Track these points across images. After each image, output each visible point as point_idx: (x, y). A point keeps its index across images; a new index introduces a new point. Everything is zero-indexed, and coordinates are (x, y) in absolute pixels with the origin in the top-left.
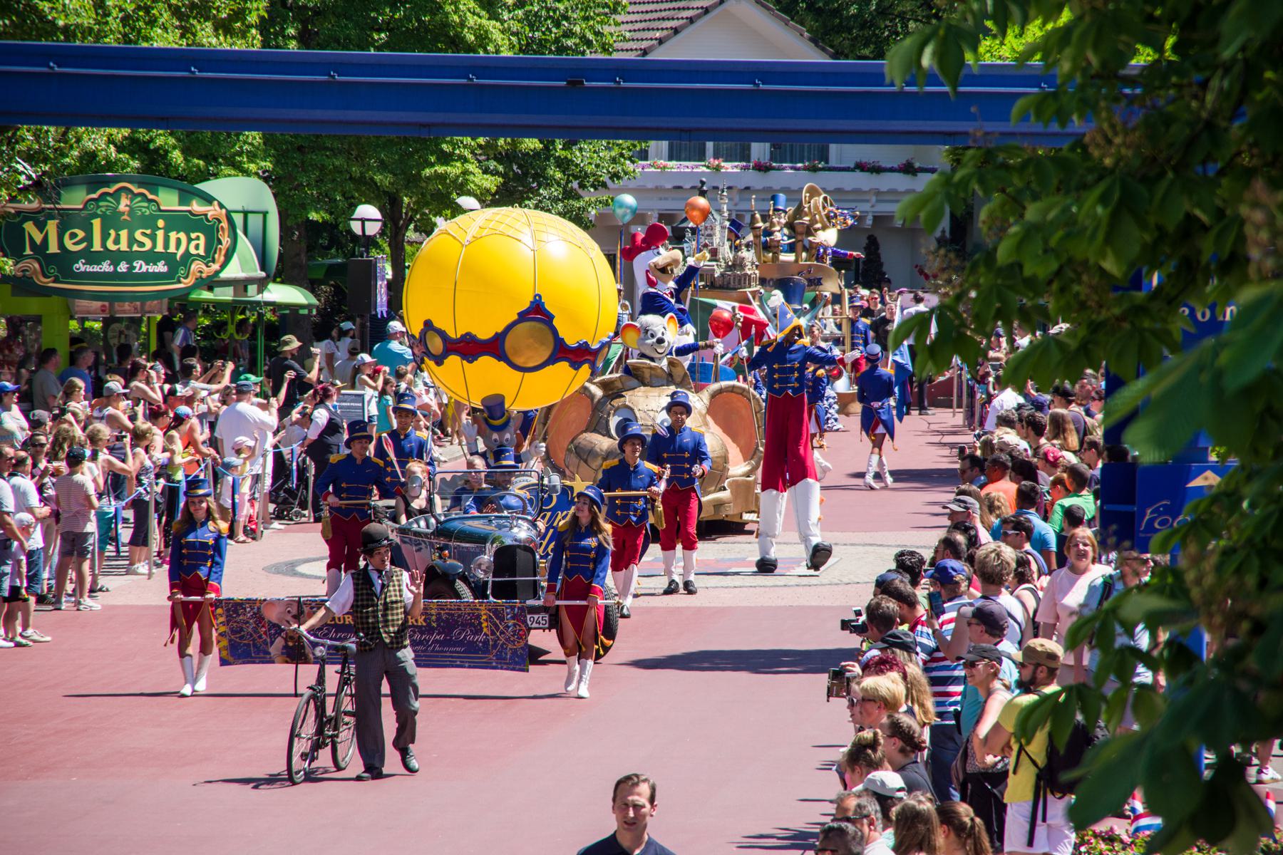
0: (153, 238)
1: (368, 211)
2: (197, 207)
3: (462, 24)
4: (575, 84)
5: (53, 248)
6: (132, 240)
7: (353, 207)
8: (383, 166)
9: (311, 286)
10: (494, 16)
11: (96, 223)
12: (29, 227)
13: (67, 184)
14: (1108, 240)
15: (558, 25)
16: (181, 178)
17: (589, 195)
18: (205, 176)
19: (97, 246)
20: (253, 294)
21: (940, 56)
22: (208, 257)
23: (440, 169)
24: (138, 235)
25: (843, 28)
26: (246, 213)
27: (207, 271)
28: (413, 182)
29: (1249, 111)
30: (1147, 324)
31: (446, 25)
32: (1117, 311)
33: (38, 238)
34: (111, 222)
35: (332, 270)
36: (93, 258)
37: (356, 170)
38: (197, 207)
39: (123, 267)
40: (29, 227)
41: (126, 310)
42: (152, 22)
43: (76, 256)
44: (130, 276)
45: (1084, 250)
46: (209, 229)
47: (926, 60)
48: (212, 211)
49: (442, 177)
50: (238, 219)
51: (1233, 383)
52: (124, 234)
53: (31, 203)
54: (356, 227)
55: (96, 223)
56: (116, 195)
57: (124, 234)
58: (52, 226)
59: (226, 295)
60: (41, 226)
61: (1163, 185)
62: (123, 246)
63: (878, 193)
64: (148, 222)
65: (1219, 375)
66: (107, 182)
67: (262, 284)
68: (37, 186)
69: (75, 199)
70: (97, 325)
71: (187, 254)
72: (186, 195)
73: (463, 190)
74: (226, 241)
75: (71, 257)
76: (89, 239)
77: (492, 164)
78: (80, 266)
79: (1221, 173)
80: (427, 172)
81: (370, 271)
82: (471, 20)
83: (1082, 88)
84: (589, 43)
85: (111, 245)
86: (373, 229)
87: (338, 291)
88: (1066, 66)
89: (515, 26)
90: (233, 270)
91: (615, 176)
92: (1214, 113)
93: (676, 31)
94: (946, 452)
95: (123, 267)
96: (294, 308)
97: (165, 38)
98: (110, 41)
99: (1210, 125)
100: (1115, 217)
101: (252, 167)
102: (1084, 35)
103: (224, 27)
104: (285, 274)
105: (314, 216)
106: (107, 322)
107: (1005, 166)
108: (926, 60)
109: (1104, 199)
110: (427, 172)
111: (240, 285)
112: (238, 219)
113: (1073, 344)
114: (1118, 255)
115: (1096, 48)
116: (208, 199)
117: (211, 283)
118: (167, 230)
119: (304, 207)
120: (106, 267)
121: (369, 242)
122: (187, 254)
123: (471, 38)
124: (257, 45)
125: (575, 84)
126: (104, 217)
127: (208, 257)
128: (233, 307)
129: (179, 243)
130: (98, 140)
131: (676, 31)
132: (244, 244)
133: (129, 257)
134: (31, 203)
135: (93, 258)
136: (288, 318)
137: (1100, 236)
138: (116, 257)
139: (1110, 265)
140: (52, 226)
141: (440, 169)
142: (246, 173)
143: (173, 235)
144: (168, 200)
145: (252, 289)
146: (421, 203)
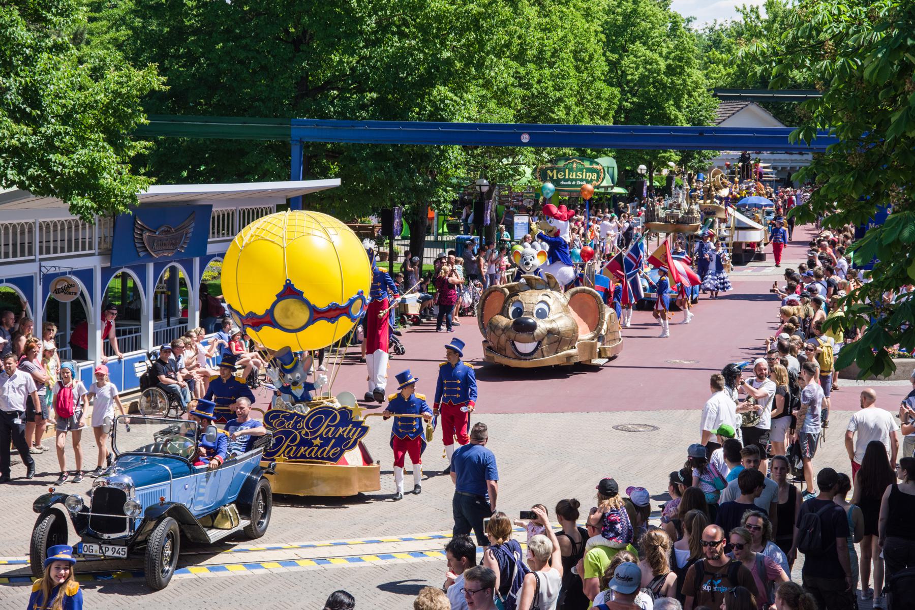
0: (582, 175)
1: (643, 167)
2: (594, 166)
3: (671, 113)
4: (701, 134)
5: (555, 178)
6: (576, 175)
7: (638, 165)
8: (647, 154)
9: (626, 188)
10: (680, 111)
11: (567, 171)
12: (549, 172)
13: (560, 160)
14: (853, 188)
15: (698, 113)
16: (590, 158)
17: (706, 162)
18: (597, 157)
19: (567, 177)
20: (609, 190)
21: (805, 135)
22: (597, 180)
23: (663, 154)
24: (578, 174)
25: (782, 113)
26: (608, 167)
27: (597, 184)
28: (655, 158)
29: (897, 151)
30: (864, 210)
31: (666, 114)
32: (856, 207)
33: (551, 175)
34: (571, 170)
35: (633, 183)
36: (566, 180)
37: (639, 155)
38: (594, 166)
39: (574, 183)
40: (549, 172)
41: (575, 195)
42: (583, 117)
43: (561, 180)
44: (576, 185)
45: (846, 191)
46: (598, 172)
47: (801, 137)
48: (599, 167)
49: (664, 157)
50: (606, 169)
51: (885, 243)
52: (574, 173)
53: (549, 165)
54: (639, 171)
55: (567, 171)
56: (573, 163)
57: (574, 173)
58: (555, 171)
59: (602, 190)
60: (552, 172)
61: (871, 173)
62: (574, 177)
63: (792, 160)
64: (581, 170)
65: (881, 240)
66: (570, 159)
67: (612, 187)
68: (550, 161)
69: (561, 164)
70: (567, 198)
71: (591, 179)
72: (592, 162)
73: (670, 160)
74: (602, 175)
75: (560, 180)
76: (565, 175)
77: (678, 153)
78: (562, 183)
79: (888, 168)
80: (660, 155)
81: (643, 183)
82: (673, 112)
83: (847, 142)
84: (707, 118)
85: (571, 177)
86: (644, 172)
87: (634, 189)
88: (842, 138)
89: (686, 114)
90: (604, 184)
91: (714, 156)
92: (885, 152)
93: (733, 114)
94: (810, 236)
95: (574, 183)
96: (621, 194)
97: (586, 122)
98: (571, 124)
99: (884, 156)
100: (855, 182)
101: (610, 154)
102: (847, 130)
103: (603, 118)
104: (619, 184)
105: (628, 168)
106: (570, 198)
107: (824, 165)
108: (801, 137)
109: (852, 176)
110: (660, 155)
111: (606, 188)
112: (606, 169)
113: (843, 216)
114: (856, 193)
115: (851, 133)
116: (598, 164)
117: (598, 187)
118: (586, 172)
119: (625, 165)
120: (569, 183)
121: (642, 175)
122: (591, 179)
123: (673, 117)
124: (611, 124)
125: (701, 134)
126: (569, 169)
127: (597, 180)
128: (604, 194)
129: (589, 176)
130: (567, 151)
131: (733, 114)
132: (607, 175)
133: (576, 180)
134: (549, 165)
135: (566, 180)
136: (620, 197)
137: (851, 187)
138: (572, 180)
139: (854, 195)
140: (555, 171)
141: (663, 154)
142: (609, 156)
143: (588, 174)
144: (587, 164)
145: (609, 189)
146: (658, 164)
